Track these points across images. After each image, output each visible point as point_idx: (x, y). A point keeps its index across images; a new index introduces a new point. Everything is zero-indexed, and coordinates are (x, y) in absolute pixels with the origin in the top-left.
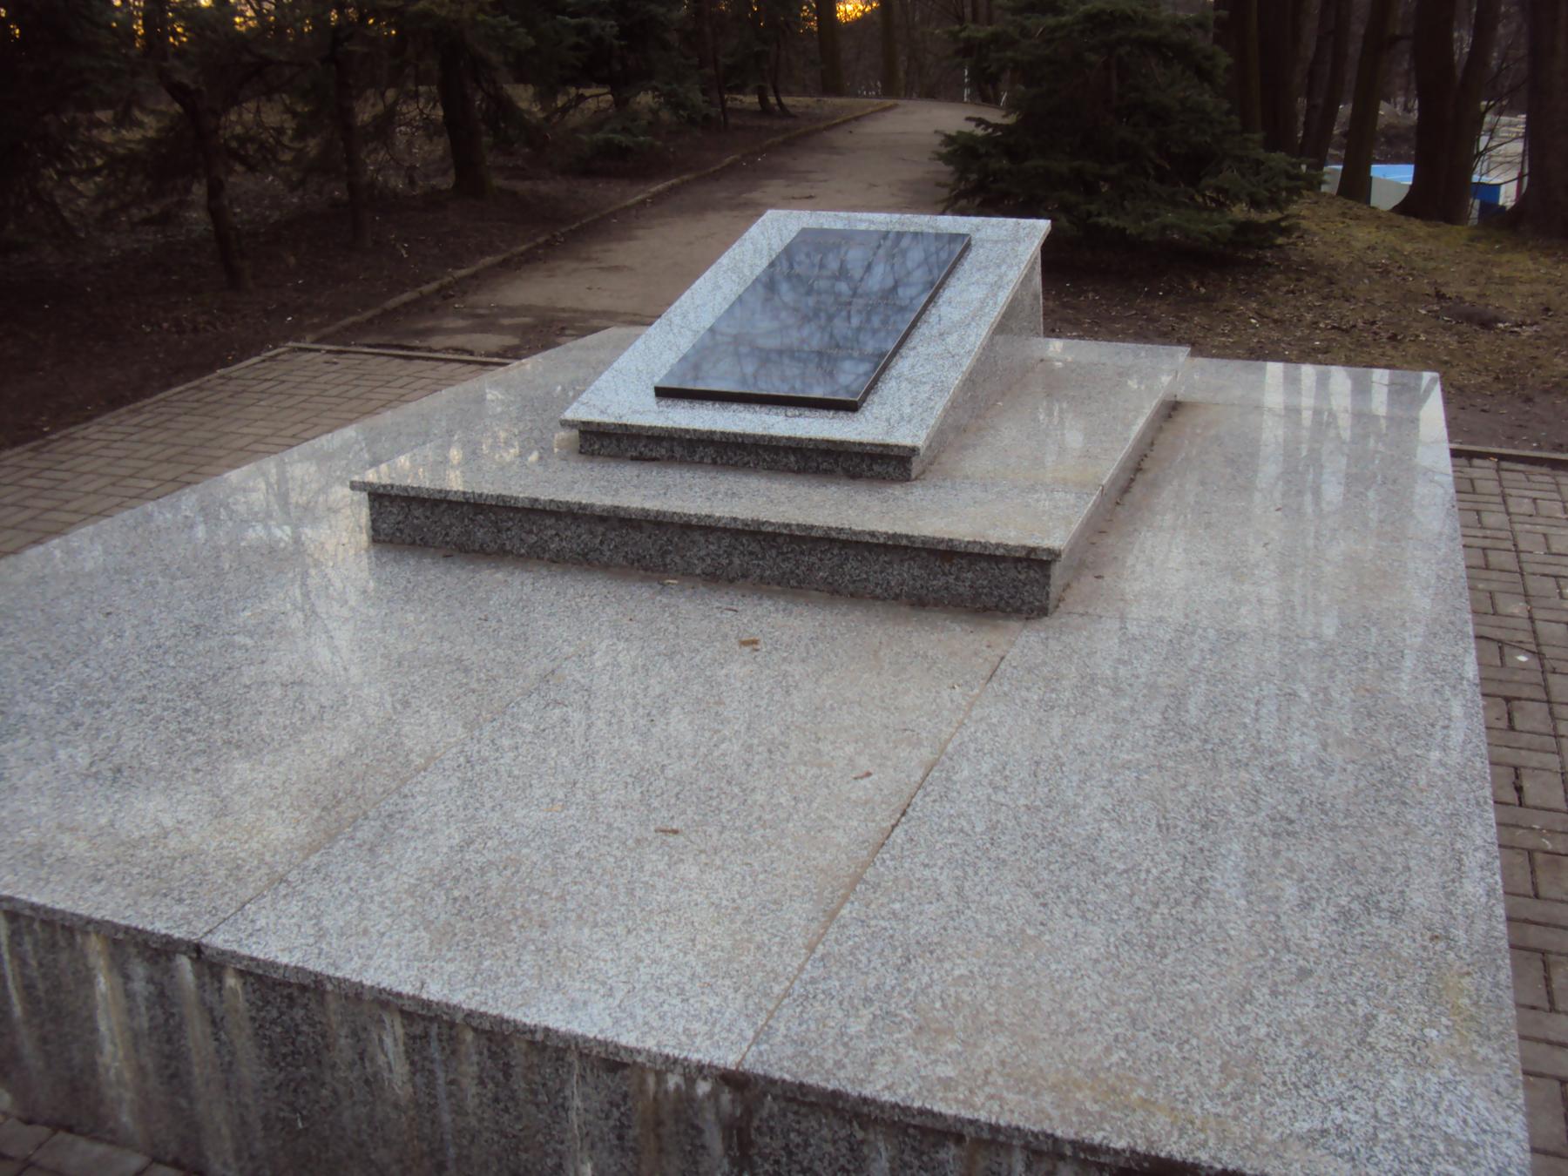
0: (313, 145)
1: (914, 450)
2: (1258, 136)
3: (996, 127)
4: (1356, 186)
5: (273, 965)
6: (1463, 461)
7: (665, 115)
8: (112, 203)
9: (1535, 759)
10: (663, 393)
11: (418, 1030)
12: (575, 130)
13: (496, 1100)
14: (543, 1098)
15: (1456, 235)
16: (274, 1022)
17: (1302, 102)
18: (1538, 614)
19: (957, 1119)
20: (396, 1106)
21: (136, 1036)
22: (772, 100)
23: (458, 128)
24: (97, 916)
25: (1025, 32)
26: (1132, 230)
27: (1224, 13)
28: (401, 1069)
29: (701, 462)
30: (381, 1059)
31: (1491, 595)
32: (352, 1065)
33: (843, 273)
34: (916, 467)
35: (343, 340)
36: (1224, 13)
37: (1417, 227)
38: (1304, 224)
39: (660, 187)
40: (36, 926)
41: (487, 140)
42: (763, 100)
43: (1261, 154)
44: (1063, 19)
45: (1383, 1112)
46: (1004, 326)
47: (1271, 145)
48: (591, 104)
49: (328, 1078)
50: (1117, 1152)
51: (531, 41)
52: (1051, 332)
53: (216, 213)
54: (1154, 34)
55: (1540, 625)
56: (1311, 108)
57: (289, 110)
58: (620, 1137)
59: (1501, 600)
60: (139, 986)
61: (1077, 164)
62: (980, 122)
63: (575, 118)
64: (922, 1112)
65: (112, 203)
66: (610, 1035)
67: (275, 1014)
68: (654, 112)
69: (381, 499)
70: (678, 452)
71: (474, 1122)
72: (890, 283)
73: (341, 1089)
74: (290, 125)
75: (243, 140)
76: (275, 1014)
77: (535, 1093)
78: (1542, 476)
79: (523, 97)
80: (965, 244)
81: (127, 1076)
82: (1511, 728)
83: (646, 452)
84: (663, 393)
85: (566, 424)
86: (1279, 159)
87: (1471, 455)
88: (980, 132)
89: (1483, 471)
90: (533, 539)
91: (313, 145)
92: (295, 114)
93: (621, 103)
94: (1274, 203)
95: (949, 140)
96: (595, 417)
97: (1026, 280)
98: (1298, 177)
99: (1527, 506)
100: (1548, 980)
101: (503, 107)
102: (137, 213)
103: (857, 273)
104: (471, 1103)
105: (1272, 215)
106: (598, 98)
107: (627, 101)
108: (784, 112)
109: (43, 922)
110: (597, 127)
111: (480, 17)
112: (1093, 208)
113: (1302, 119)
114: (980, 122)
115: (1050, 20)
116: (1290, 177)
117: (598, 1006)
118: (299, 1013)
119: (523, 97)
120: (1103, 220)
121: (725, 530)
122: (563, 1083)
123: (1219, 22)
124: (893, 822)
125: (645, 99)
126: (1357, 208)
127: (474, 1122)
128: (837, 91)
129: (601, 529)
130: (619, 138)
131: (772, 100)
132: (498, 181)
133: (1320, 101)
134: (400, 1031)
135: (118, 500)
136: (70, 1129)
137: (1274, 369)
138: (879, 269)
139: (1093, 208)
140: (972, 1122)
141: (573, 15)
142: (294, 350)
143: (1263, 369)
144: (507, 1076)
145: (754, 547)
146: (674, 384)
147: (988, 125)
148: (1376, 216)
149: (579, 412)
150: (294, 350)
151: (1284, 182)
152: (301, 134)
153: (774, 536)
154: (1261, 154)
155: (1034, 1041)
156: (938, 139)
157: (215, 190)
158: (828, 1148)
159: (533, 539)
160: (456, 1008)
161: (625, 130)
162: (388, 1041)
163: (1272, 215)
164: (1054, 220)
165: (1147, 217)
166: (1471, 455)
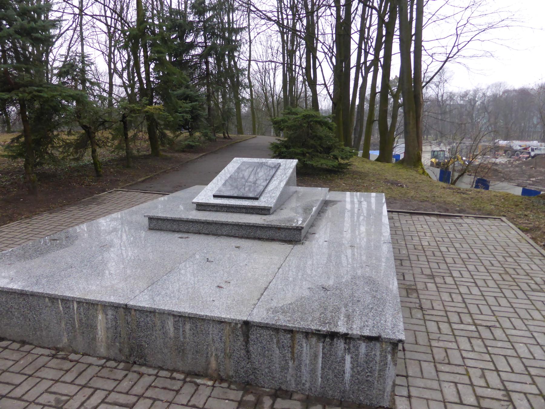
0: (116, 142)
1: (271, 207)
2: (343, 143)
3: (283, 141)
4: (366, 155)
5: (145, 307)
6: (390, 213)
7: (202, 138)
8: (66, 154)
9: (407, 271)
10: (215, 196)
11: (176, 319)
12: (180, 141)
13: (193, 334)
14: (204, 332)
15: (388, 166)
16: (143, 322)
17: (353, 136)
18: (407, 243)
19: (292, 327)
20: (170, 338)
21: (108, 329)
22: (226, 135)
23: (152, 139)
24: (102, 300)
25: (289, 119)
26: (314, 164)
27: (335, 115)
28: (172, 329)
29: (224, 211)
30: (167, 328)
31: (397, 240)
32: (160, 330)
33: (243, 177)
34: (271, 212)
35: (130, 188)
36: (335, 115)
37: (379, 163)
38: (354, 163)
39: (201, 155)
40: (85, 305)
41: (159, 143)
42: (224, 135)
43: (343, 147)
44: (298, 116)
45: (375, 323)
46: (288, 184)
47: (346, 145)
48: (184, 135)
49: (154, 334)
50: (324, 331)
51: (172, 119)
52: (298, 185)
53: (94, 157)
54: (319, 120)
55: (408, 246)
56: (355, 137)
57: (110, 133)
58: (221, 339)
59: (399, 241)
60: (110, 316)
61: (302, 149)
62: (279, 140)
63: (179, 138)
64: (285, 326)
65: (66, 154)
66: (220, 316)
67: (143, 319)
68: (200, 137)
69: (151, 219)
70: (219, 209)
71: (188, 340)
72: (255, 179)
73: (157, 336)
74: (111, 136)
75: (99, 140)
76: (143, 319)
77: (202, 331)
78: (408, 217)
79: (169, 133)
80: (279, 165)
81: (104, 340)
82: (402, 265)
83: (211, 209)
84: (215, 196)
85: (193, 203)
86: (348, 148)
87: (392, 212)
88: (279, 142)
89: (395, 215)
90: (187, 228)
91: (116, 142)
92: (112, 134)
93: (191, 135)
94: (347, 158)
95: (272, 144)
96: (200, 201)
97: (292, 173)
98: (352, 152)
99: (405, 222)
100: (411, 313)
101: (164, 135)
102: (71, 157)
103: (246, 178)
104: (188, 335)
105: (346, 161)
106: (185, 134)
107: (193, 134)
108: (229, 138)
109: (87, 303)
110: (186, 140)
111: (161, 113)
112: (305, 160)
113: (353, 140)
114: (279, 140)
115: (295, 116)
116: (350, 152)
117: (216, 311)
118: (149, 319)
119: (169, 133)
120: (308, 162)
121: (231, 224)
122: (209, 328)
123: (334, 117)
124: (278, 266)
125: (197, 134)
126: (365, 159)
127: (188, 340)
128: (242, 134)
129: (202, 225)
130: (191, 143)
131: (226, 135)
132: (162, 153)
133: (357, 136)
134: (172, 320)
135: (55, 232)
136: (87, 355)
137: (348, 194)
138: (252, 177)
139: (305, 160)
140: (295, 327)
141: (180, 113)
142: (115, 191)
143: (346, 194)
144: (196, 328)
145: (237, 228)
146: (218, 194)
147: (281, 140)
148: (371, 161)
149: (195, 200)
150: (115, 191)
151: (349, 154)
152: (113, 139)
153: (242, 225)
154: (343, 147)
155: (306, 314)
156: (269, 144)
157: (94, 151)
158: (265, 337)
159: (187, 228)
160: (187, 313)
161: (193, 141)
162: (169, 323)
163: (346, 161)
164: (299, 160)
165: (318, 161)
166: (392, 212)
